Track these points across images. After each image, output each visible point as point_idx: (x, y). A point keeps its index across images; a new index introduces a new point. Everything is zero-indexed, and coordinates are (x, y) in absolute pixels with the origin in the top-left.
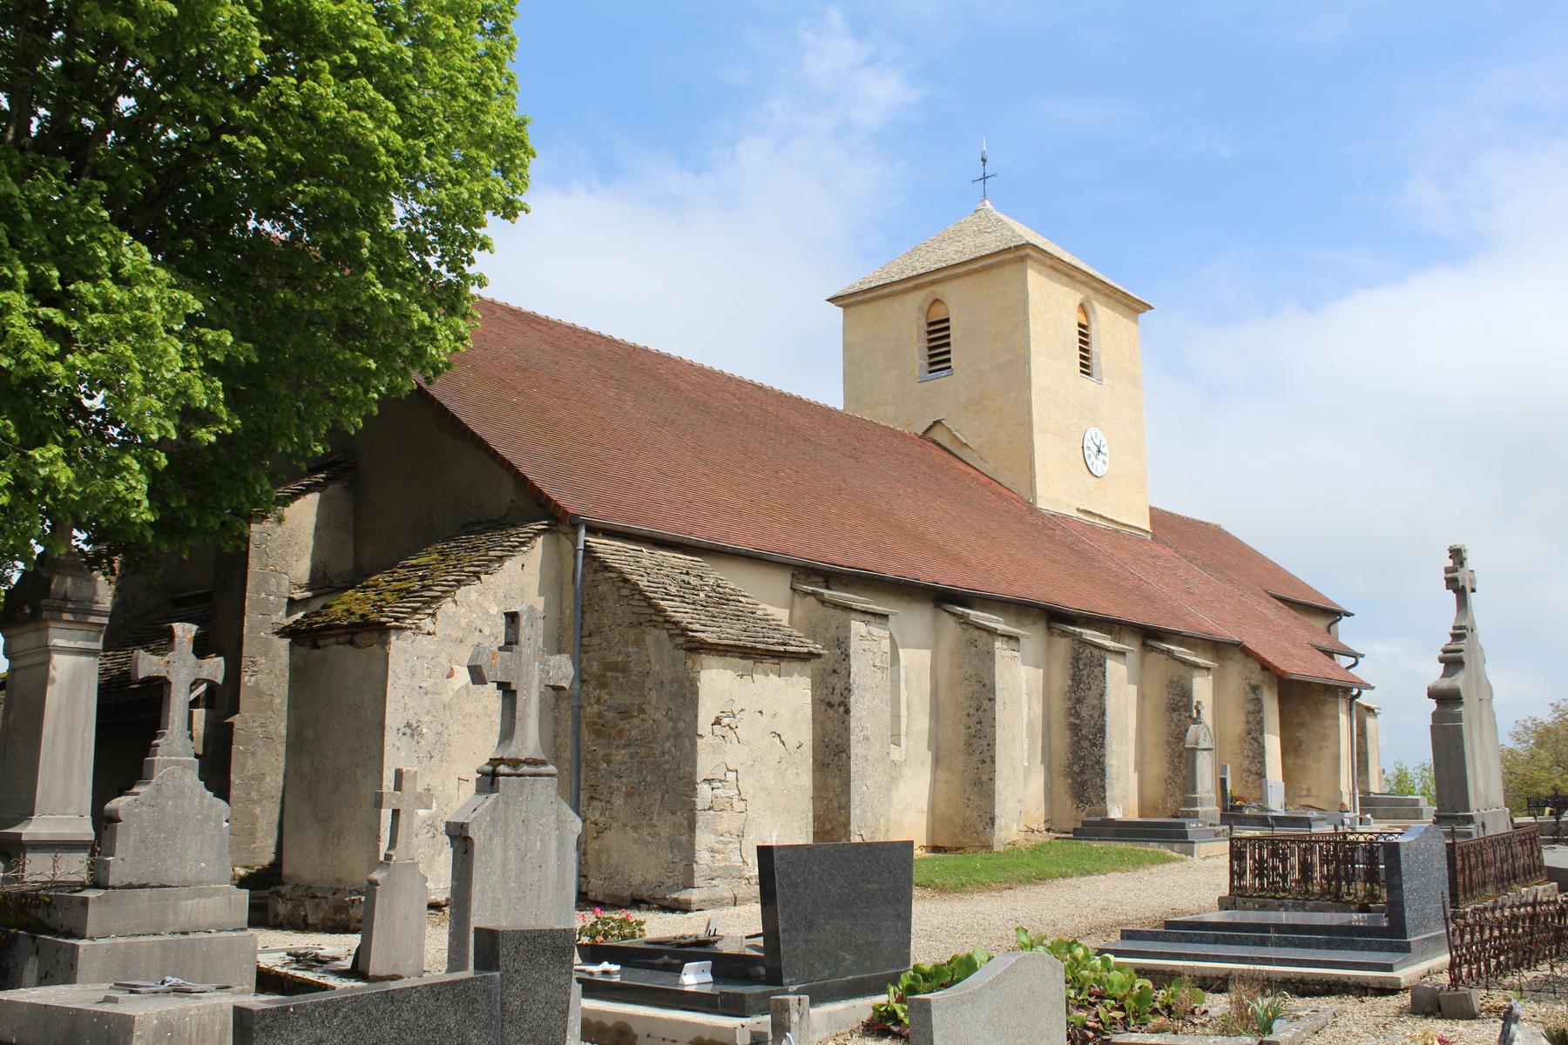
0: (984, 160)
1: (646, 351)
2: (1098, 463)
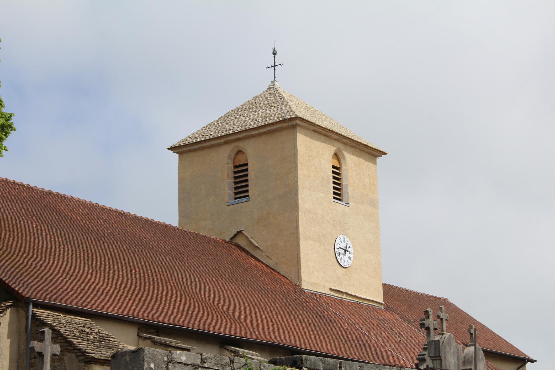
0: (274, 54)
1: (50, 193)
2: (346, 258)
